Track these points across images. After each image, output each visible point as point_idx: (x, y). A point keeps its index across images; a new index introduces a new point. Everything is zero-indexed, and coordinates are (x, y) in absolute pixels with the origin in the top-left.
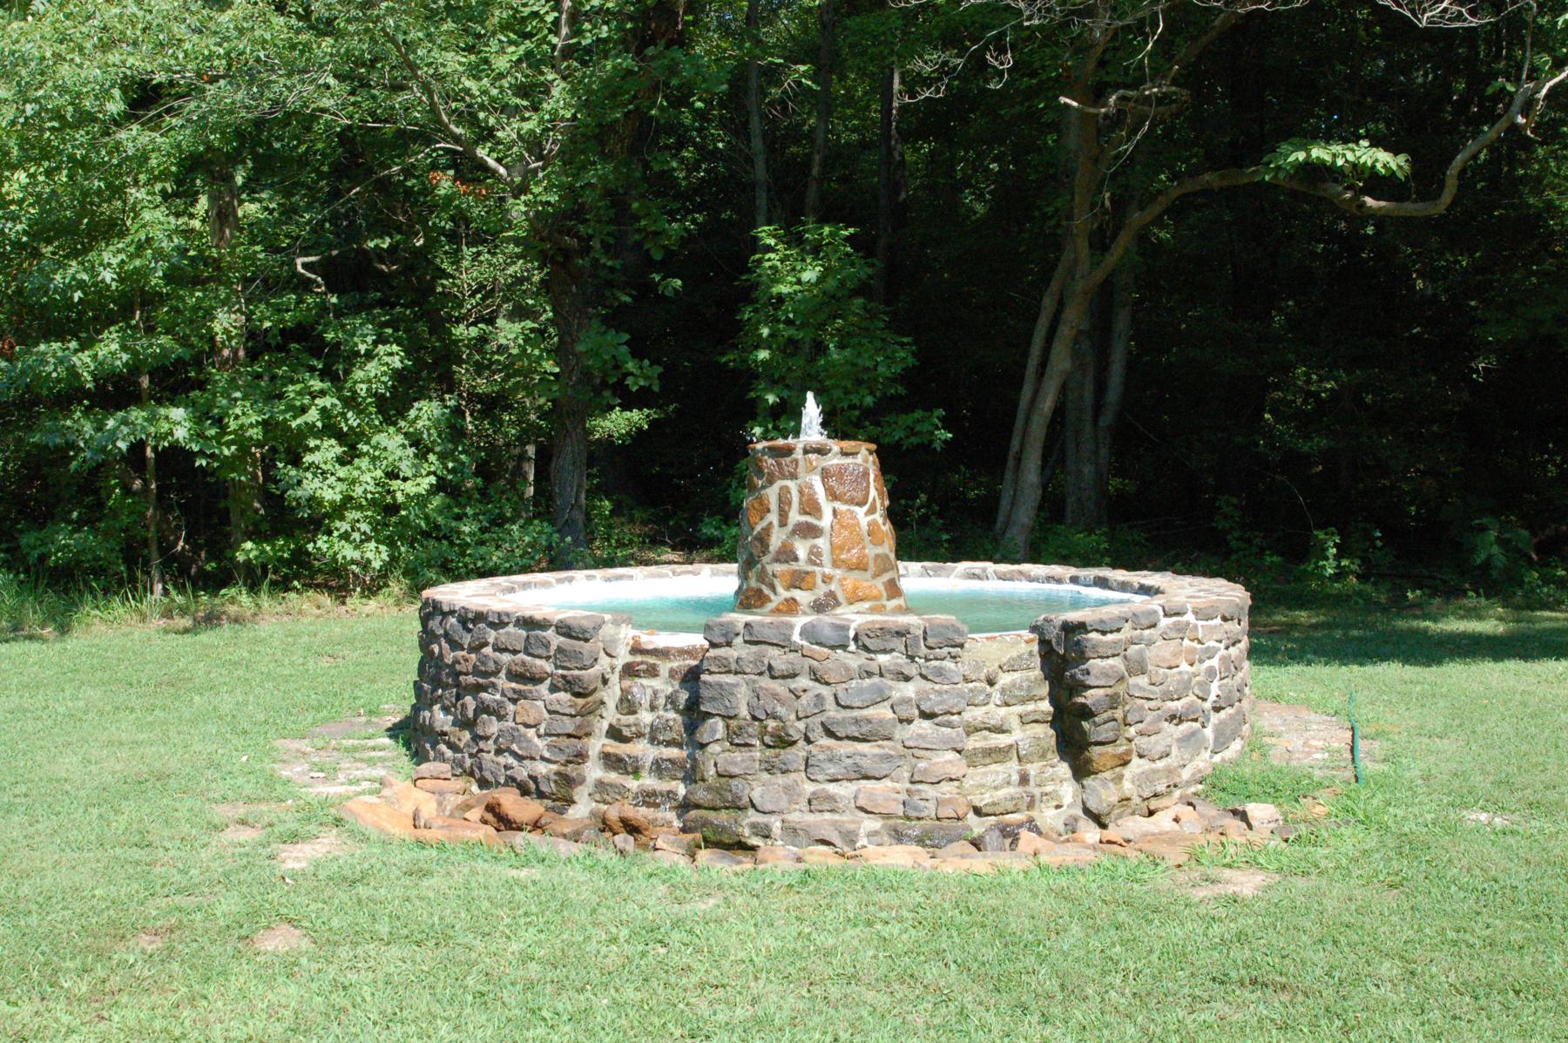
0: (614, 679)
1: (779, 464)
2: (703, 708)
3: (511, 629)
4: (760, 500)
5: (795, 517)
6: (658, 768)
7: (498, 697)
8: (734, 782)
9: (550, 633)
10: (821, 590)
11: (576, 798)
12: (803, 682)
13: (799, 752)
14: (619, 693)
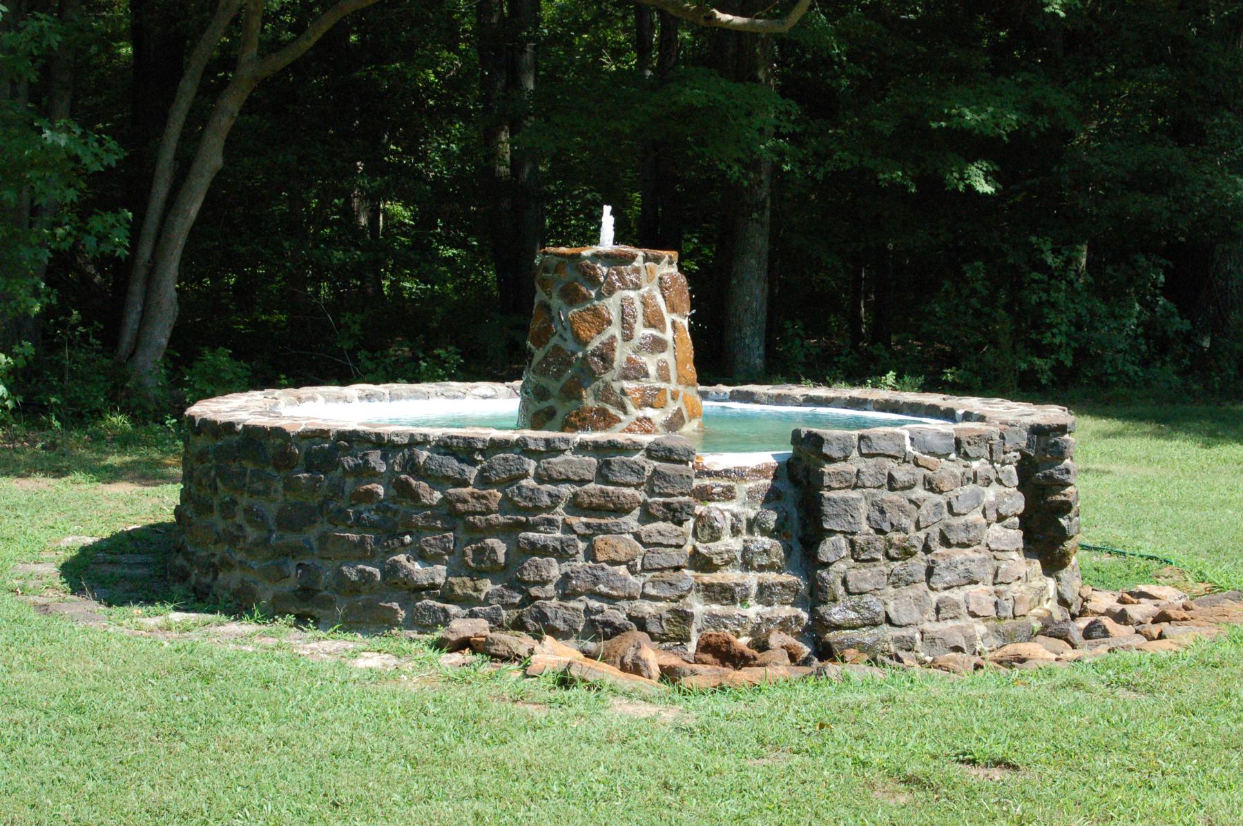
1: (619, 273)
2: (826, 526)
3: (569, 455)
4: (596, 313)
5: (642, 332)
6: (765, 594)
7: (558, 534)
8: (867, 598)
9: (638, 457)
10: (673, 407)
12: (919, 492)
13: (918, 564)
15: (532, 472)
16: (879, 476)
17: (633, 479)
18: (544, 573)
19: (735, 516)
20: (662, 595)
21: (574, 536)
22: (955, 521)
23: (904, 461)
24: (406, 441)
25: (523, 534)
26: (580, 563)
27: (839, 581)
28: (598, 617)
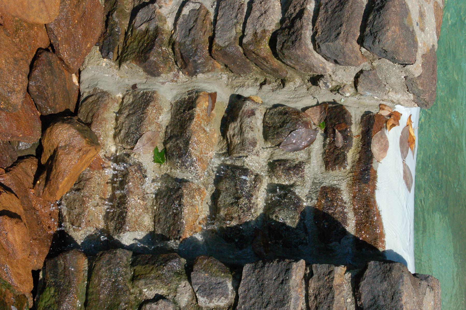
0: (324, 95)
2: (247, 268)
6: (172, 194)
11: (125, 66)
14: (299, 105)
19: (298, 167)
20: (181, 20)
27: (163, 291)
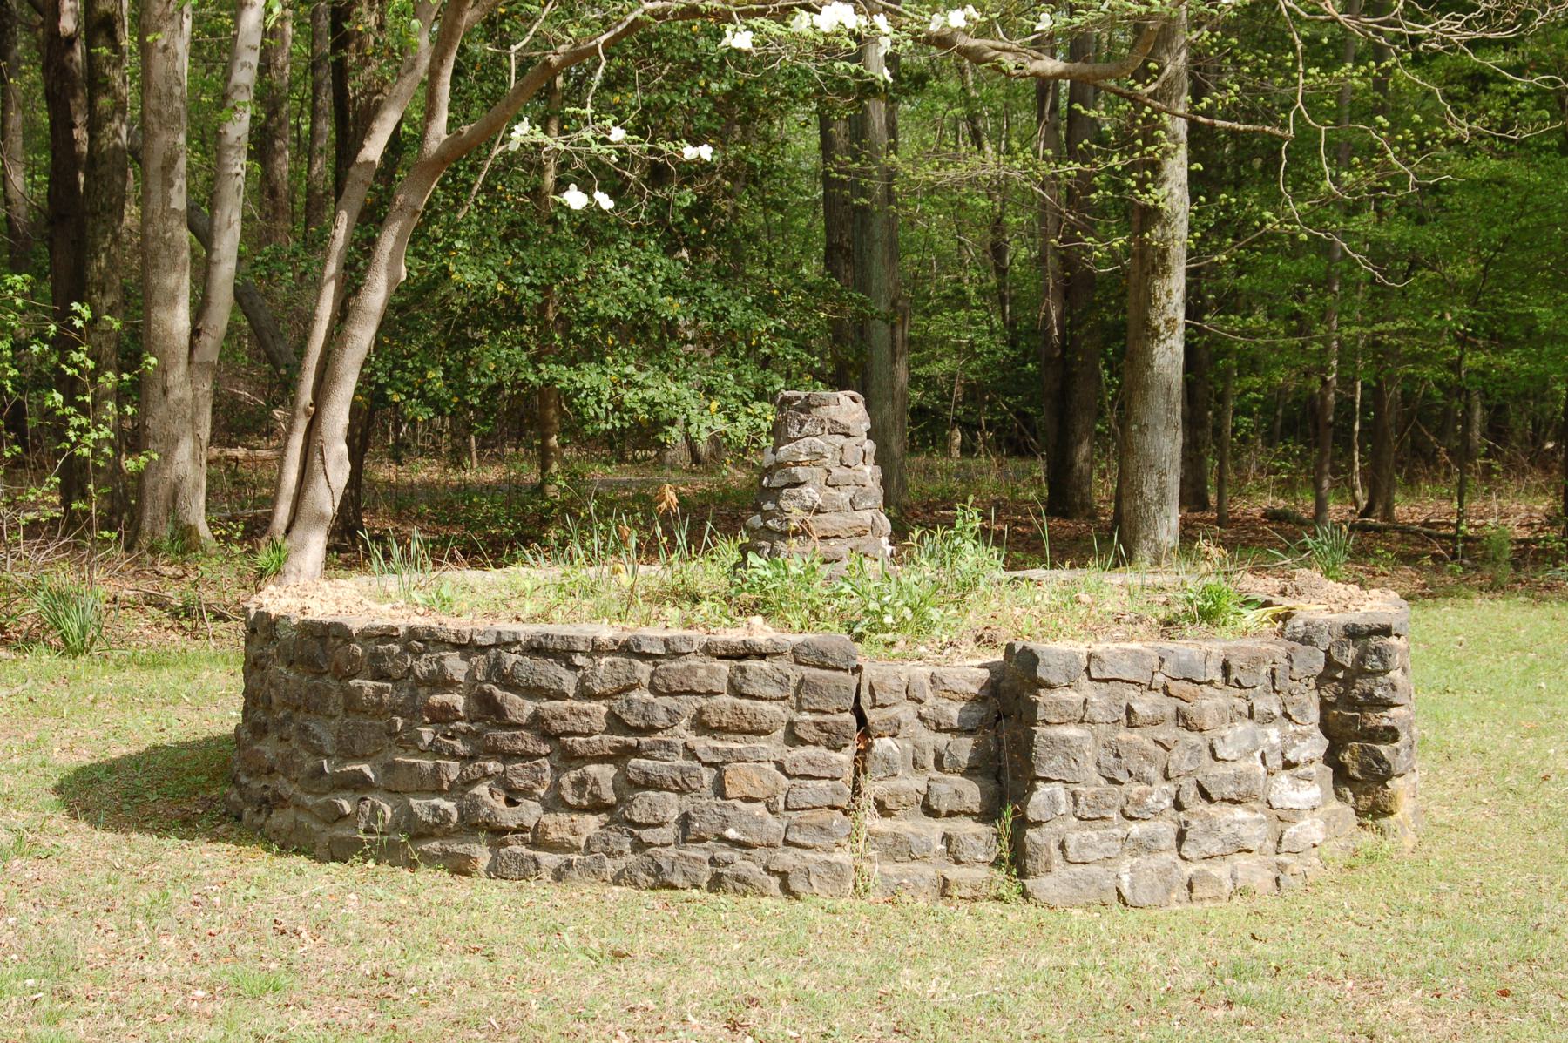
7: (680, 762)
15: (645, 680)
16: (1115, 710)
17: (773, 691)
18: (660, 813)
20: (810, 843)
21: (695, 764)
22: (1219, 769)
23: (1150, 689)
24: (492, 641)
25: (633, 761)
26: (708, 800)
28: (726, 871)
